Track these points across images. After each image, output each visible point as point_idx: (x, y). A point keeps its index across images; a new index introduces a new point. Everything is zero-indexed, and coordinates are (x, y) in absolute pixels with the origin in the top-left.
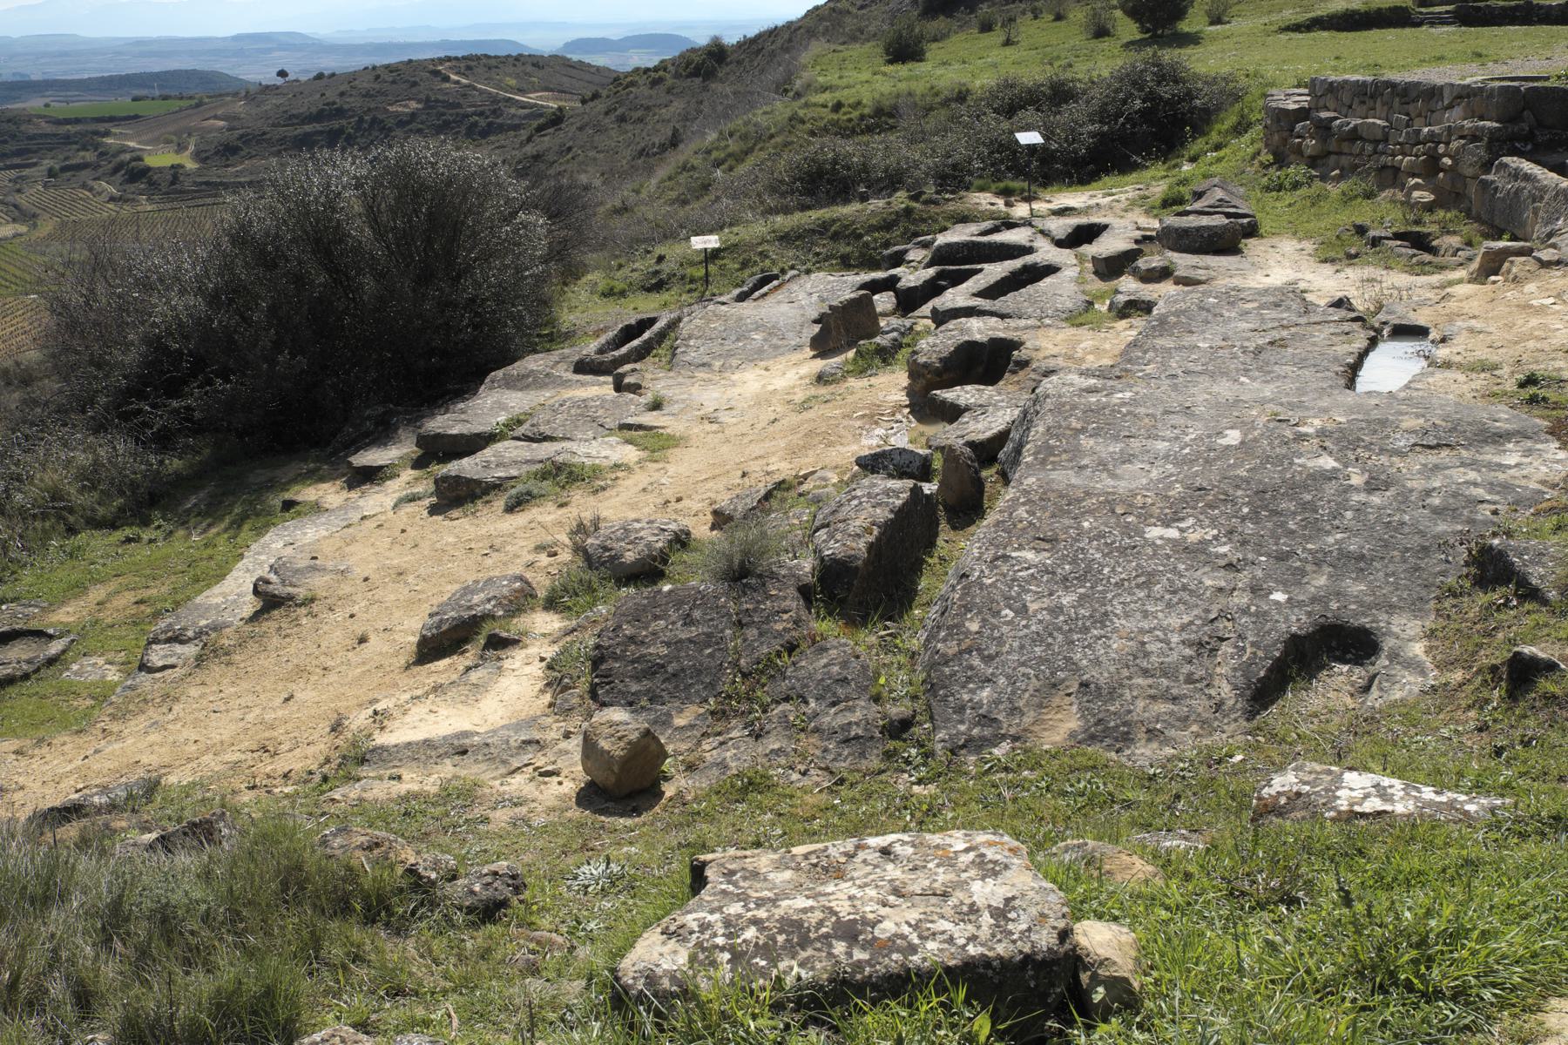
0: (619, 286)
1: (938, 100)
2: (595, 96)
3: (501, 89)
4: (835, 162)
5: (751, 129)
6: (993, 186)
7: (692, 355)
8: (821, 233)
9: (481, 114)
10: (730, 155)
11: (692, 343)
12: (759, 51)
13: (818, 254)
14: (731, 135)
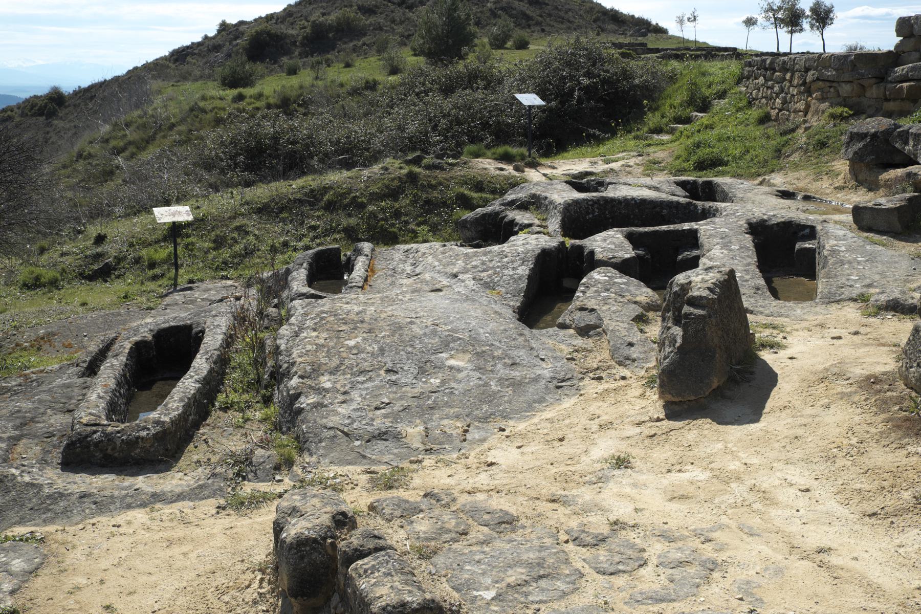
0: (48, 274)
1: (344, 90)
6: (489, 153)
7: (340, 414)
8: (311, 204)
10: (130, 143)
11: (326, 382)
12: (92, 98)
13: (314, 228)
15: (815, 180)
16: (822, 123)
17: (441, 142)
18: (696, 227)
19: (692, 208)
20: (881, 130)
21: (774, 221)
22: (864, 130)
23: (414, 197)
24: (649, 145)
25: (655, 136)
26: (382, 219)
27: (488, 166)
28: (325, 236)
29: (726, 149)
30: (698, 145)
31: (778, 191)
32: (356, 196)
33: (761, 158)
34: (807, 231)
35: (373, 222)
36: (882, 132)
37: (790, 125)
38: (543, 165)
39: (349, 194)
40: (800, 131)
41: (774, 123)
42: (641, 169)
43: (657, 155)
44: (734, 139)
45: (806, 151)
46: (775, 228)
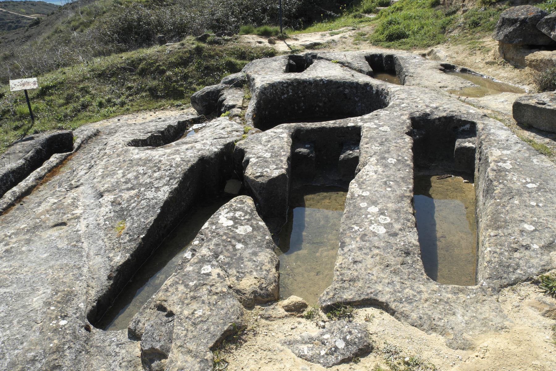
2: (53, 13)
3: (20, 13)
4: (139, 20)
5: (93, 9)
6: (255, 31)
8: (131, 71)
9: (13, 22)
10: (81, 24)
13: (130, 88)
14: (82, 13)
15: (471, 55)
16: (476, 7)
17: (236, 22)
18: (360, 124)
19: (368, 88)
20: (529, 16)
21: (437, 115)
22: (514, 16)
23: (199, 64)
24: (361, 22)
25: (367, 15)
26: (175, 81)
27: (251, 41)
28: (136, 94)
29: (408, 25)
30: (390, 23)
31: (442, 65)
32: (160, 65)
33: (431, 33)
34: (468, 126)
35: (168, 83)
36: (530, 18)
37: (452, 8)
38: (290, 38)
39: (155, 63)
40: (460, 13)
41: (442, 6)
42: (352, 40)
43: (365, 29)
44: (415, 18)
45: (464, 29)
46: (437, 122)
